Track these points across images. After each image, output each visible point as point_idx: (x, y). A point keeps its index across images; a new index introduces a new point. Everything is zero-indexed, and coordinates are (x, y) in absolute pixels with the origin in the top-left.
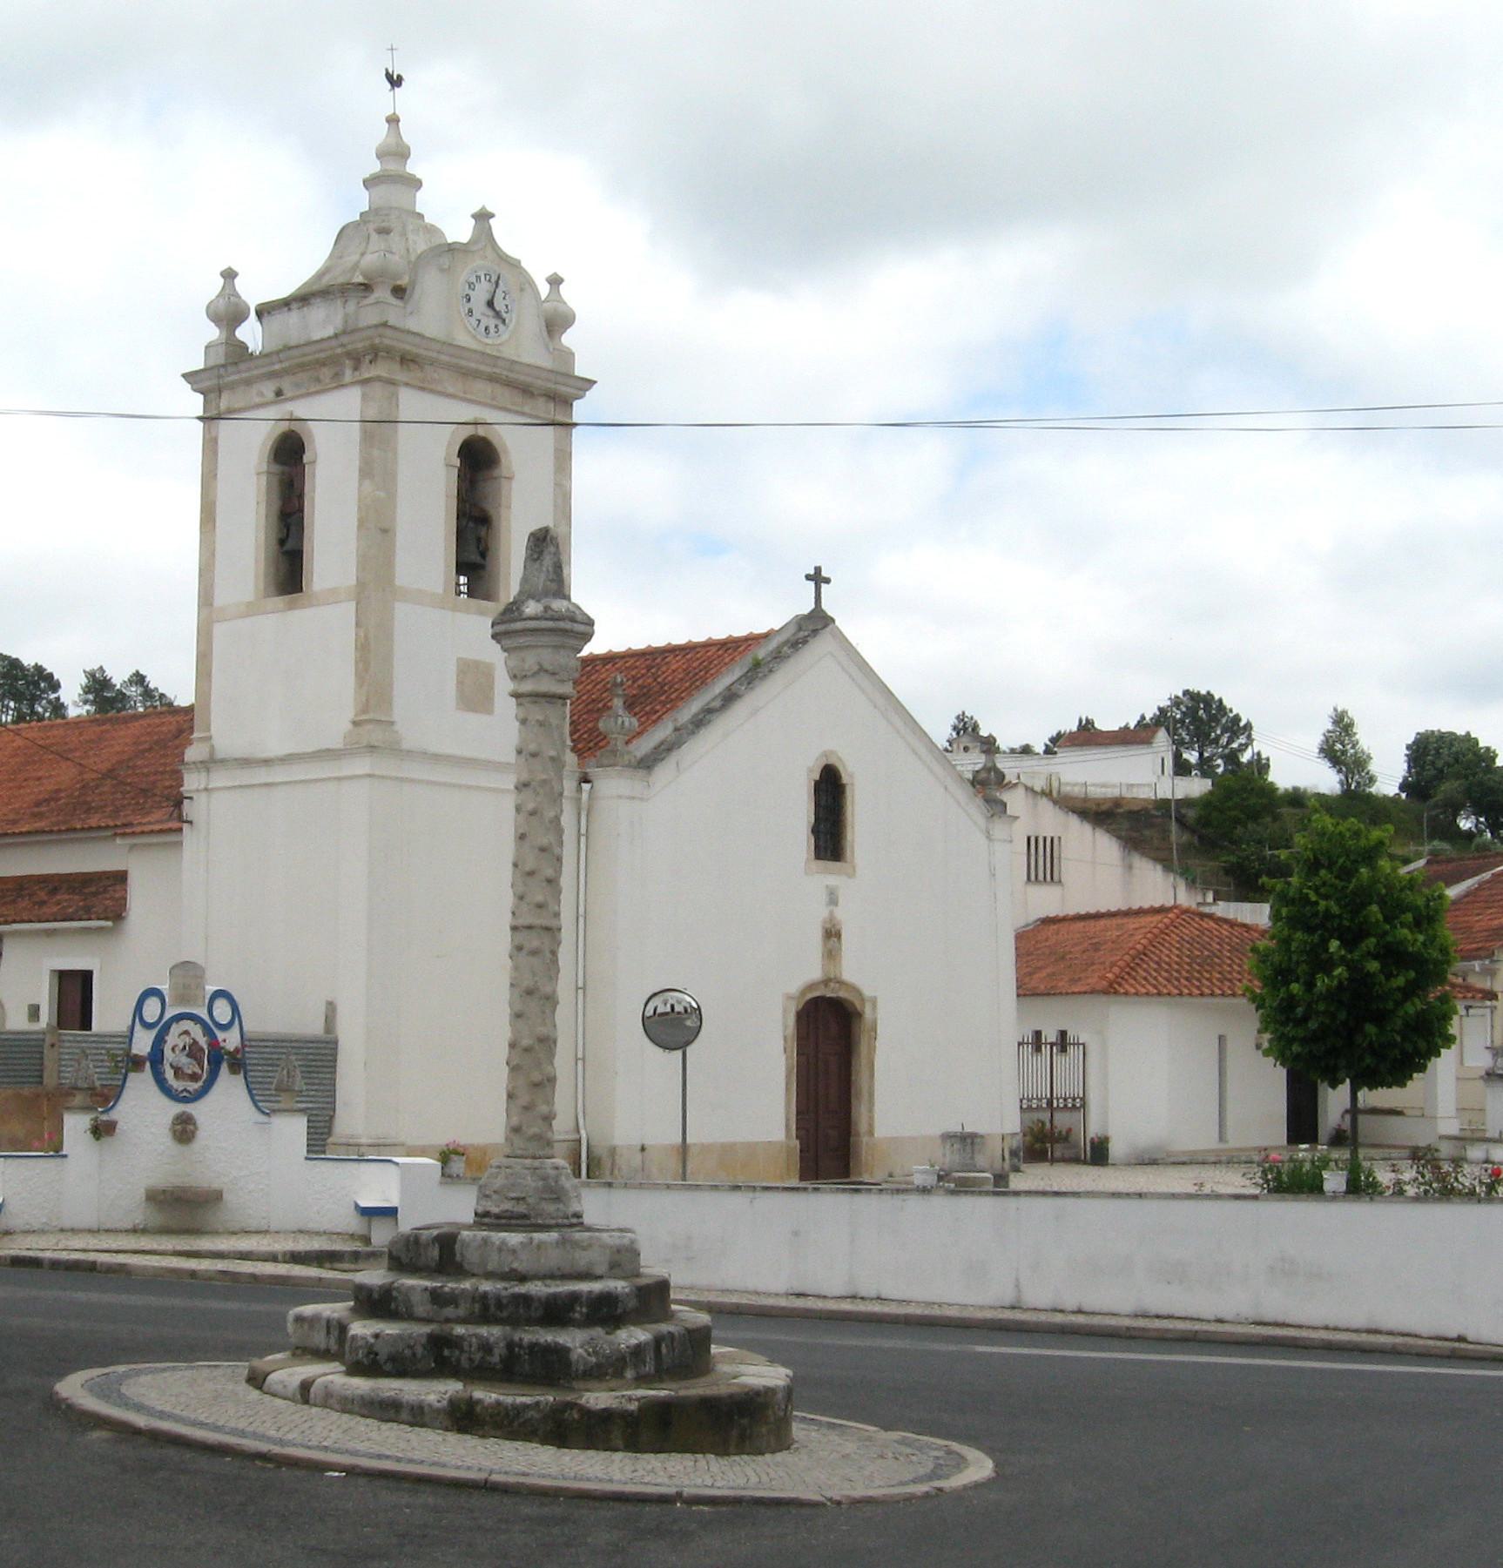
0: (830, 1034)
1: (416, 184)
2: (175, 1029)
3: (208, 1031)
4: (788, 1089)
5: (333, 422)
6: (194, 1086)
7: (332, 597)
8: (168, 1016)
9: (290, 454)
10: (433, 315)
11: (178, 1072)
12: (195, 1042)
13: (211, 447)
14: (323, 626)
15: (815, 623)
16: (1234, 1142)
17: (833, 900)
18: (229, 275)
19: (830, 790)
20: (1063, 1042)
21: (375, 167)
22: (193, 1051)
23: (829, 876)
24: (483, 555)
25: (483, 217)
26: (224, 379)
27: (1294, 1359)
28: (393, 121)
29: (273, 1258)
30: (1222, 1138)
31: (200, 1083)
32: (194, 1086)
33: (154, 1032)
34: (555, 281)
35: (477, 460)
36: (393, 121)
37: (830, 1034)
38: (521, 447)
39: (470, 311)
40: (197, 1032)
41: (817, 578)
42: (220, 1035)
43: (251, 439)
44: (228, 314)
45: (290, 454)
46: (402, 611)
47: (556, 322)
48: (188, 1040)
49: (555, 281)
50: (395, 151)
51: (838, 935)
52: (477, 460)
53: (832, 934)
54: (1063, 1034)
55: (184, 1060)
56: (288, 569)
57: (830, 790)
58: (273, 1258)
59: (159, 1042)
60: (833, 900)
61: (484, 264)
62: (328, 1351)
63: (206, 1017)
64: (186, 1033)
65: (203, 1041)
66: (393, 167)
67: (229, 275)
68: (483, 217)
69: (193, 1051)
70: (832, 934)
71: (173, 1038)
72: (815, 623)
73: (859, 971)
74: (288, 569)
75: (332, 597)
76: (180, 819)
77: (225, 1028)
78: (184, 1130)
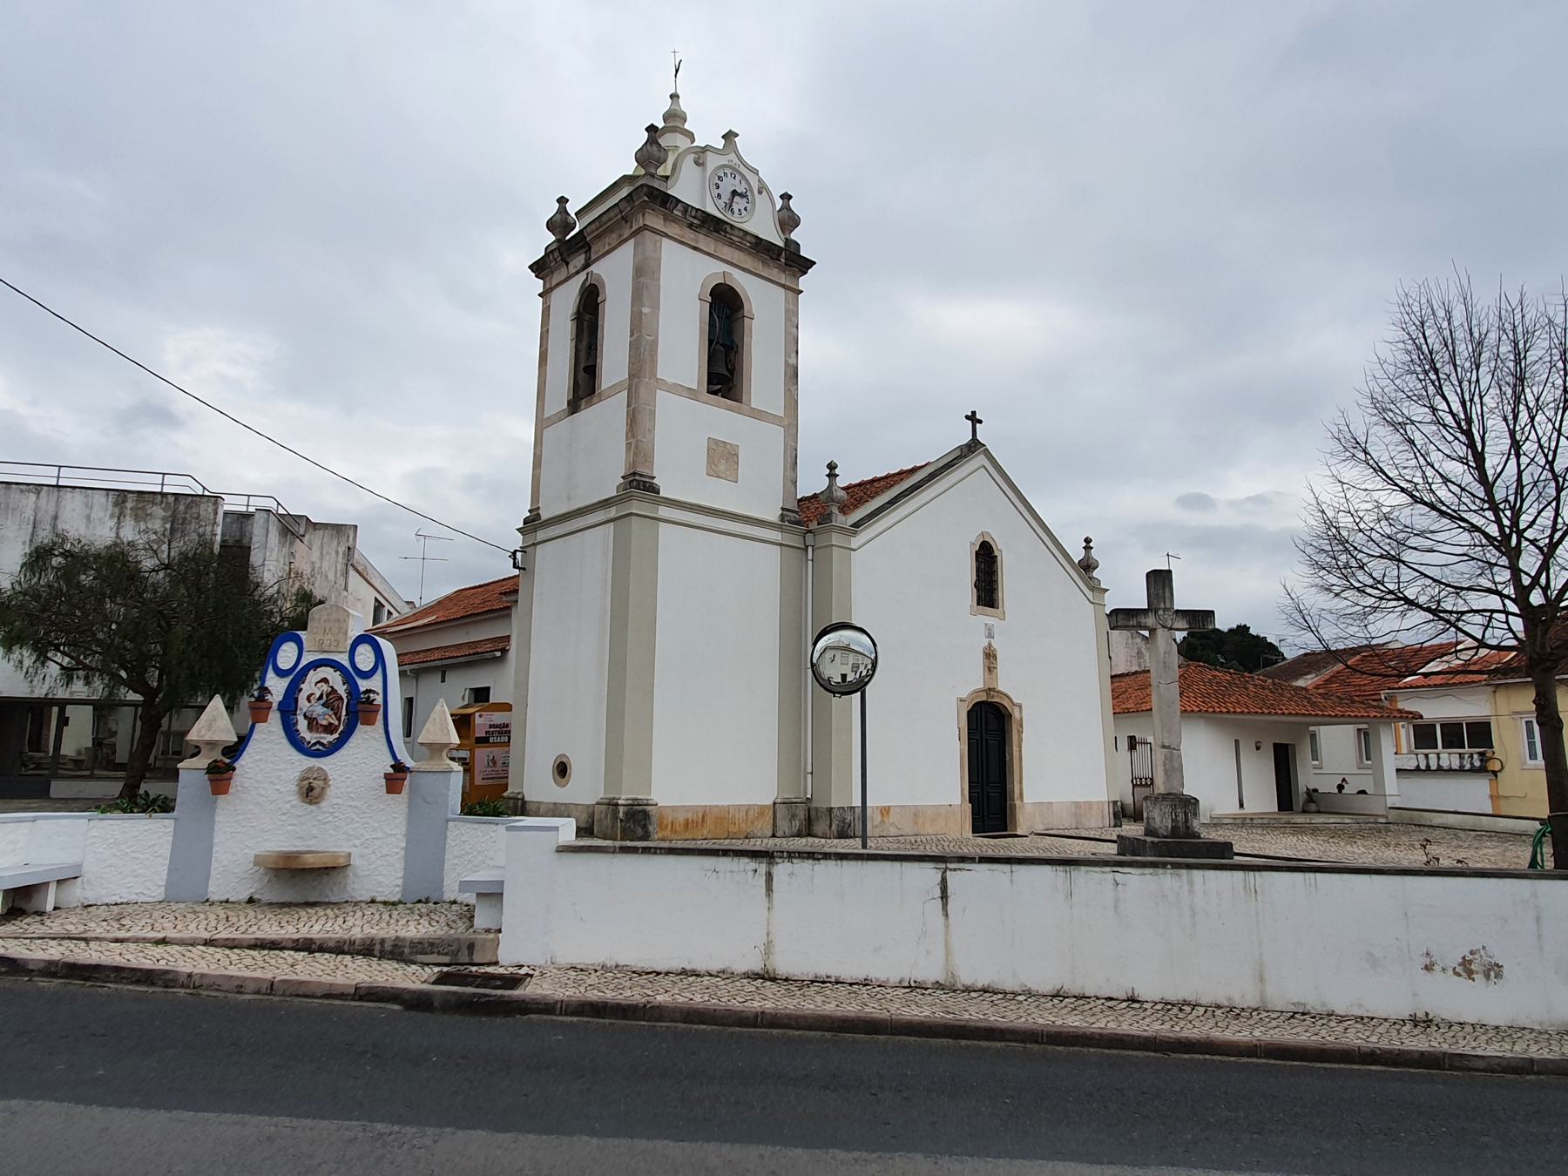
0: (990, 731)
2: (313, 676)
3: (348, 679)
4: (962, 778)
6: (328, 738)
7: (615, 390)
8: (304, 662)
10: (688, 188)
11: (312, 723)
12: (333, 691)
14: (608, 414)
15: (974, 446)
16: (1250, 808)
18: (562, 201)
19: (986, 558)
22: (330, 700)
23: (986, 618)
24: (732, 372)
25: (729, 136)
28: (674, 97)
30: (1241, 806)
31: (336, 735)
32: (328, 738)
33: (287, 680)
35: (725, 308)
36: (674, 97)
37: (990, 731)
38: (760, 295)
39: (719, 196)
40: (336, 679)
41: (973, 418)
42: (363, 685)
43: (568, 296)
44: (559, 223)
46: (663, 399)
47: (788, 221)
48: (325, 688)
49: (786, 197)
51: (995, 657)
52: (725, 308)
53: (990, 655)
55: (319, 710)
57: (986, 558)
60: (990, 635)
62: (1418, 769)
63: (346, 663)
64: (325, 680)
65: (342, 690)
67: (562, 201)
68: (729, 136)
69: (330, 700)
70: (990, 655)
71: (309, 686)
72: (974, 446)
73: (1012, 685)
74: (585, 385)
75: (615, 390)
78: (311, 792)
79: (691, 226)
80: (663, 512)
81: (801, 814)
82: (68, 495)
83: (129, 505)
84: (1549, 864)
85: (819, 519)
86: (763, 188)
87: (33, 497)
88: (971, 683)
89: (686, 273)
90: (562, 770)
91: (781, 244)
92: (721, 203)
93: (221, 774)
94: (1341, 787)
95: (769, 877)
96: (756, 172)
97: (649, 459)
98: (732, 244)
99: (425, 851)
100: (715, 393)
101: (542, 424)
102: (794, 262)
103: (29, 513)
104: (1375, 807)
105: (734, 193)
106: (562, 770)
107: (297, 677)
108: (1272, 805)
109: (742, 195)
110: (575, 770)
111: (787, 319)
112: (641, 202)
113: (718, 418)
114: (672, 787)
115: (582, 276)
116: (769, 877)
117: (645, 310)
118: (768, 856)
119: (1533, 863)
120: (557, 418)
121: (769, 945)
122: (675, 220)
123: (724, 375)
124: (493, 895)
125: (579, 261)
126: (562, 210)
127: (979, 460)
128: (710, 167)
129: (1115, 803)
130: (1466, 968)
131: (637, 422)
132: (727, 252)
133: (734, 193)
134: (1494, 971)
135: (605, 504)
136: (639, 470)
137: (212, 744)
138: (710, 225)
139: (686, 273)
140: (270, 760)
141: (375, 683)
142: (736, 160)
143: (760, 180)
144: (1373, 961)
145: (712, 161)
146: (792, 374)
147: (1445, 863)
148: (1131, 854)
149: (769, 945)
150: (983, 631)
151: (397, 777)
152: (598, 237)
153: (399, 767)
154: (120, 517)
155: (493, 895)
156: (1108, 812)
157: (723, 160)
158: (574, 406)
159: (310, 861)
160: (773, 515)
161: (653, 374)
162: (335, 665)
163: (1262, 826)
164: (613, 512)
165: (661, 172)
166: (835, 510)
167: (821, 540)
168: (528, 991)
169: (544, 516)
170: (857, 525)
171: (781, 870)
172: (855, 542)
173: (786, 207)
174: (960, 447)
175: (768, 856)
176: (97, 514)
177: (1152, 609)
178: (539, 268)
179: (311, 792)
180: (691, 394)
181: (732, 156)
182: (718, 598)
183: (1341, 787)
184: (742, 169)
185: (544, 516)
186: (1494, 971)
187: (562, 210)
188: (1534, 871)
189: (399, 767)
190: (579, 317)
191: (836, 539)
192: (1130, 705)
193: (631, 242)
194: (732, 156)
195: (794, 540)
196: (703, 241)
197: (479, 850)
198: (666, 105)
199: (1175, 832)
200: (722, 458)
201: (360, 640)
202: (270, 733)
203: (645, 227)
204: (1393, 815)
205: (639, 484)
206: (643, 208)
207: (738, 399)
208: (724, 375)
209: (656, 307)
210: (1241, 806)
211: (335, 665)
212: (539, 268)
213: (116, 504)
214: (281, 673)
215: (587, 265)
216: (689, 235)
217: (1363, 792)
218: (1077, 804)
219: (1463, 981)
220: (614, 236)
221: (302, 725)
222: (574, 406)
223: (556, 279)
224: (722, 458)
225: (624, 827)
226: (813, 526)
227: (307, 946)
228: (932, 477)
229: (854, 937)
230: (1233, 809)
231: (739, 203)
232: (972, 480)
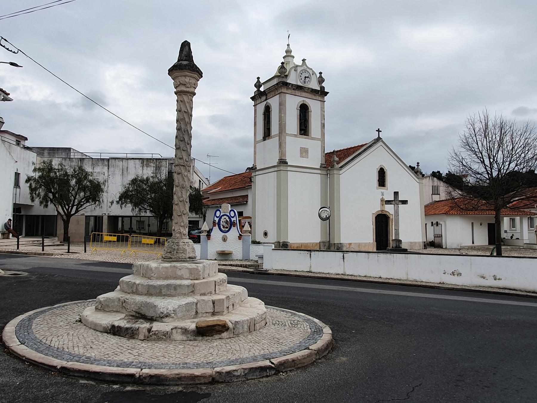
1: (293, 57)
2: (223, 218)
3: (229, 218)
5: (274, 102)
9: (267, 111)
10: (292, 80)
11: (223, 226)
13: (255, 111)
14: (273, 142)
15: (379, 139)
16: (476, 244)
17: (383, 195)
18: (258, 78)
19: (382, 173)
20: (437, 224)
21: (285, 54)
22: (227, 222)
23: (382, 190)
25: (304, 60)
26: (258, 96)
27: (524, 301)
28: (288, 45)
29: (236, 266)
30: (473, 243)
34: (321, 73)
35: (304, 110)
36: (288, 45)
37: (382, 223)
38: (313, 105)
41: (379, 131)
42: (233, 219)
43: (261, 108)
44: (258, 85)
45: (267, 111)
47: (321, 80)
49: (321, 73)
50: (288, 51)
52: (304, 110)
54: (437, 222)
55: (225, 224)
56: (267, 134)
57: (382, 173)
58: (236, 266)
59: (220, 220)
60: (383, 195)
61: (305, 70)
65: (228, 220)
66: (288, 54)
67: (258, 78)
68: (304, 60)
71: (222, 220)
72: (379, 139)
74: (267, 134)
76: (251, 181)
77: (233, 217)
78: (224, 240)
79: (294, 89)
80: (289, 168)
81: (327, 245)
82: (130, 161)
83: (145, 163)
84: (495, 254)
85: (335, 161)
86: (314, 73)
87: (121, 162)
88: (377, 208)
89: (293, 102)
90: (266, 234)
91: (319, 89)
92: (302, 81)
93: (209, 236)
94: (512, 237)
95: (310, 254)
96: (311, 69)
97: (285, 155)
98: (305, 92)
99: (246, 251)
100: (302, 134)
101: (256, 142)
102: (323, 93)
103: (121, 167)
104: (520, 243)
105: (305, 77)
106: (266, 234)
107: (220, 218)
108: (486, 243)
109: (308, 77)
110: (269, 234)
111: (321, 110)
112: (281, 83)
113: (303, 141)
114: (293, 239)
115: (265, 103)
116: (310, 254)
117: (283, 115)
118: (310, 251)
119: (491, 254)
120: (259, 142)
121: (310, 266)
122: (289, 88)
123: (304, 128)
124: (261, 257)
125: (264, 98)
126: (258, 81)
127: (380, 143)
128: (299, 71)
129: (424, 242)
130: (453, 274)
131: (281, 145)
132: (304, 94)
133: (305, 77)
134: (459, 274)
135: (274, 167)
136: (283, 158)
137: (205, 231)
138: (299, 88)
139: (293, 102)
140: (216, 233)
141: (234, 219)
142: (306, 67)
143: (313, 71)
144: (432, 272)
145: (299, 69)
146: (323, 126)
147: (464, 254)
148: (108, 160)
149: (310, 266)
150: (381, 194)
151: (240, 237)
152: (269, 93)
153: (240, 235)
154: (143, 167)
155: (261, 257)
156: (422, 245)
157: (302, 68)
158: (264, 139)
159: (226, 252)
160: (318, 167)
161: (285, 132)
162: (227, 216)
163: (478, 249)
164: (276, 169)
165: (286, 74)
166: (335, 164)
167: (331, 172)
168: (269, 272)
169: (258, 169)
170: (341, 167)
171: (313, 253)
172: (341, 172)
173: (321, 77)
174: (375, 140)
175: (310, 251)
176: (137, 166)
177: (394, 200)
178: (253, 98)
179: (224, 240)
180: (295, 136)
181: (305, 67)
182: (304, 191)
183: (512, 237)
184: (308, 70)
185: (258, 169)
186: (459, 274)
187: (258, 81)
188: (491, 256)
189: (240, 235)
190: (265, 114)
191: (335, 172)
192: (437, 212)
193: (278, 96)
194: (305, 67)
195: (325, 173)
196: (297, 93)
197: (255, 251)
198: (286, 48)
199: (396, 247)
200: (304, 152)
201: (231, 211)
202: (216, 229)
203: (282, 92)
204: (525, 246)
205: (283, 162)
206: (281, 86)
207: (308, 135)
208: (304, 128)
209: (285, 114)
210: (473, 243)
211: (227, 216)
212: (253, 98)
213: (141, 163)
214: (217, 217)
215: (266, 100)
216: (293, 92)
217: (518, 239)
218: (411, 243)
219: (452, 276)
220: (273, 93)
221: (222, 227)
222: (264, 139)
223: (258, 102)
224: (304, 152)
225: (283, 246)
226: (330, 168)
227: (231, 265)
228: (370, 146)
229: (328, 265)
230: (470, 244)
231: (307, 79)
232: (378, 149)
